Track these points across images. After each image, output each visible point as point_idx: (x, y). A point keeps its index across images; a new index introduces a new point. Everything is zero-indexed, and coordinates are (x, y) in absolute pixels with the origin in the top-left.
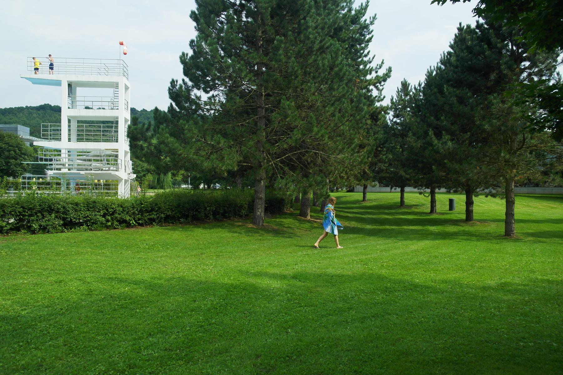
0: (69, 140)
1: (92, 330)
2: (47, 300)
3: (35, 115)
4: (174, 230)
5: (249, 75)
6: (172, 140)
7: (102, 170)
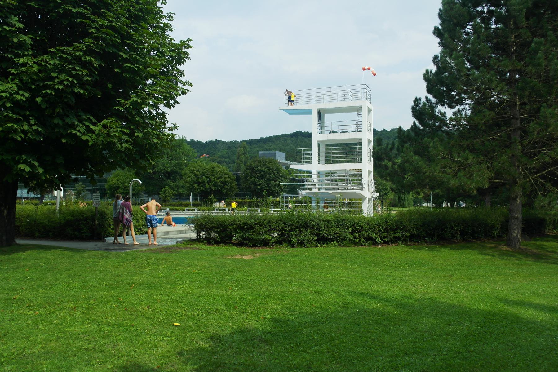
0: (319, 162)
1: (350, 341)
2: (309, 309)
3: (289, 142)
4: (420, 249)
5: (500, 85)
6: (416, 158)
7: (347, 189)
